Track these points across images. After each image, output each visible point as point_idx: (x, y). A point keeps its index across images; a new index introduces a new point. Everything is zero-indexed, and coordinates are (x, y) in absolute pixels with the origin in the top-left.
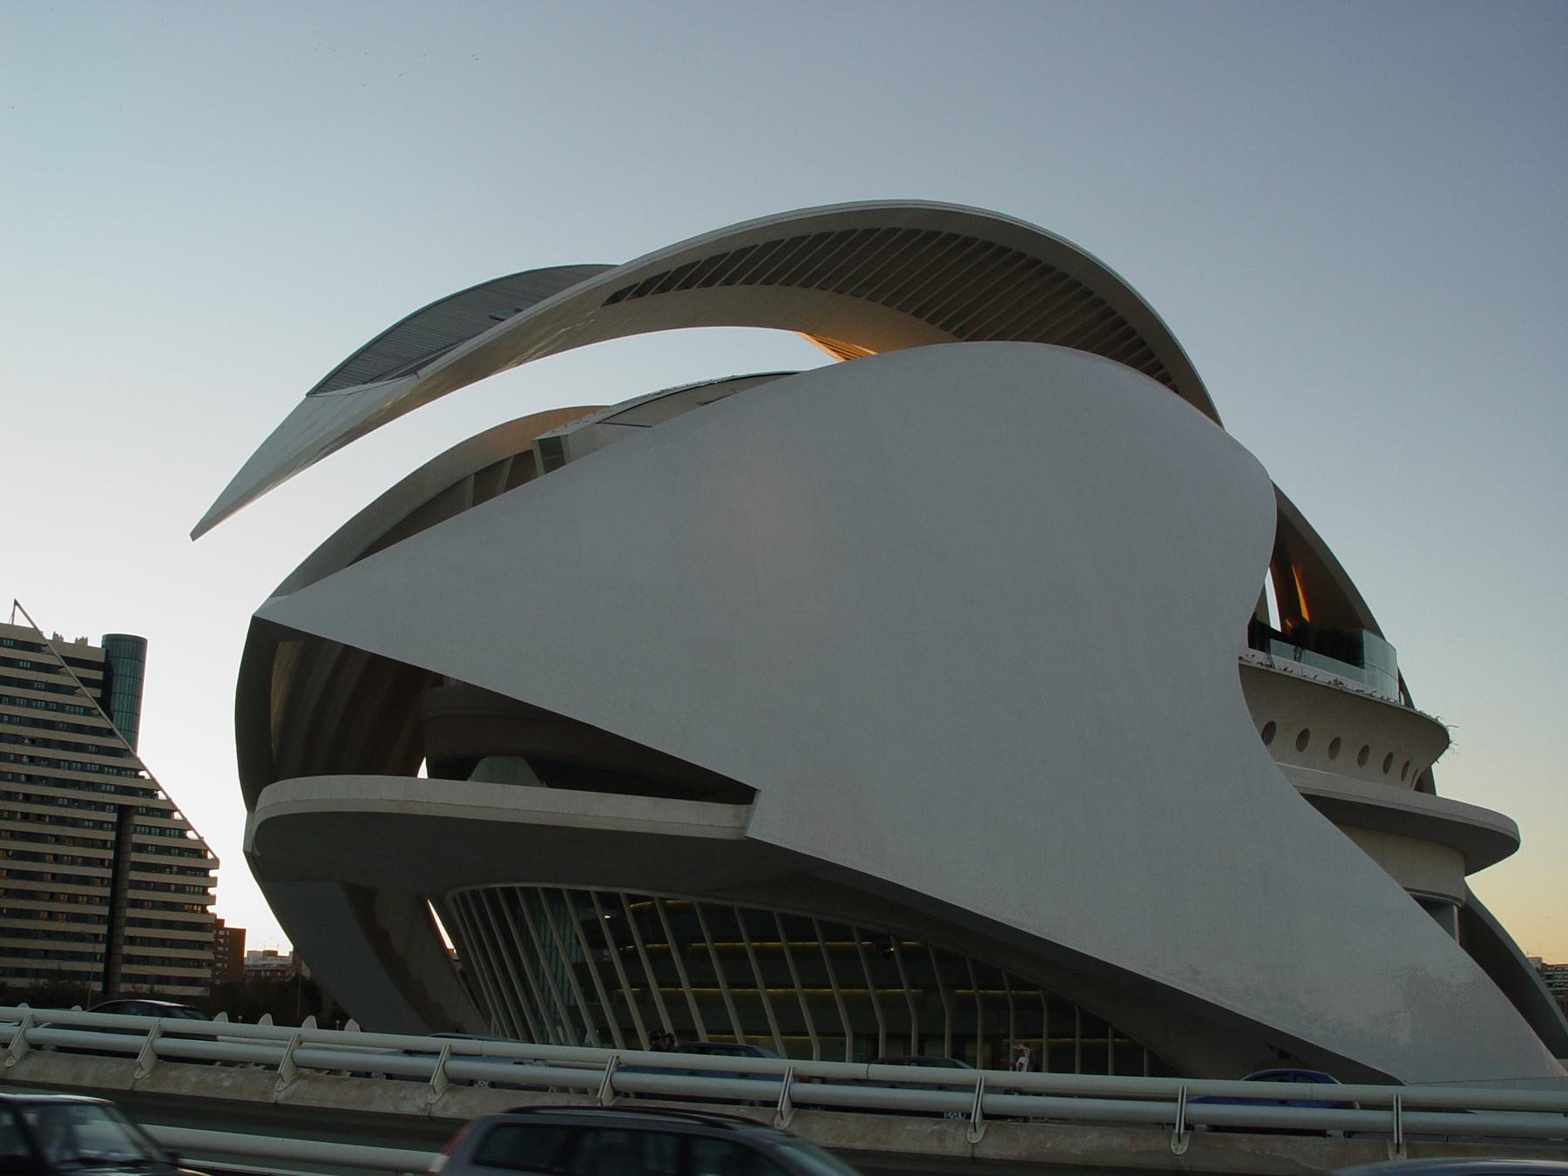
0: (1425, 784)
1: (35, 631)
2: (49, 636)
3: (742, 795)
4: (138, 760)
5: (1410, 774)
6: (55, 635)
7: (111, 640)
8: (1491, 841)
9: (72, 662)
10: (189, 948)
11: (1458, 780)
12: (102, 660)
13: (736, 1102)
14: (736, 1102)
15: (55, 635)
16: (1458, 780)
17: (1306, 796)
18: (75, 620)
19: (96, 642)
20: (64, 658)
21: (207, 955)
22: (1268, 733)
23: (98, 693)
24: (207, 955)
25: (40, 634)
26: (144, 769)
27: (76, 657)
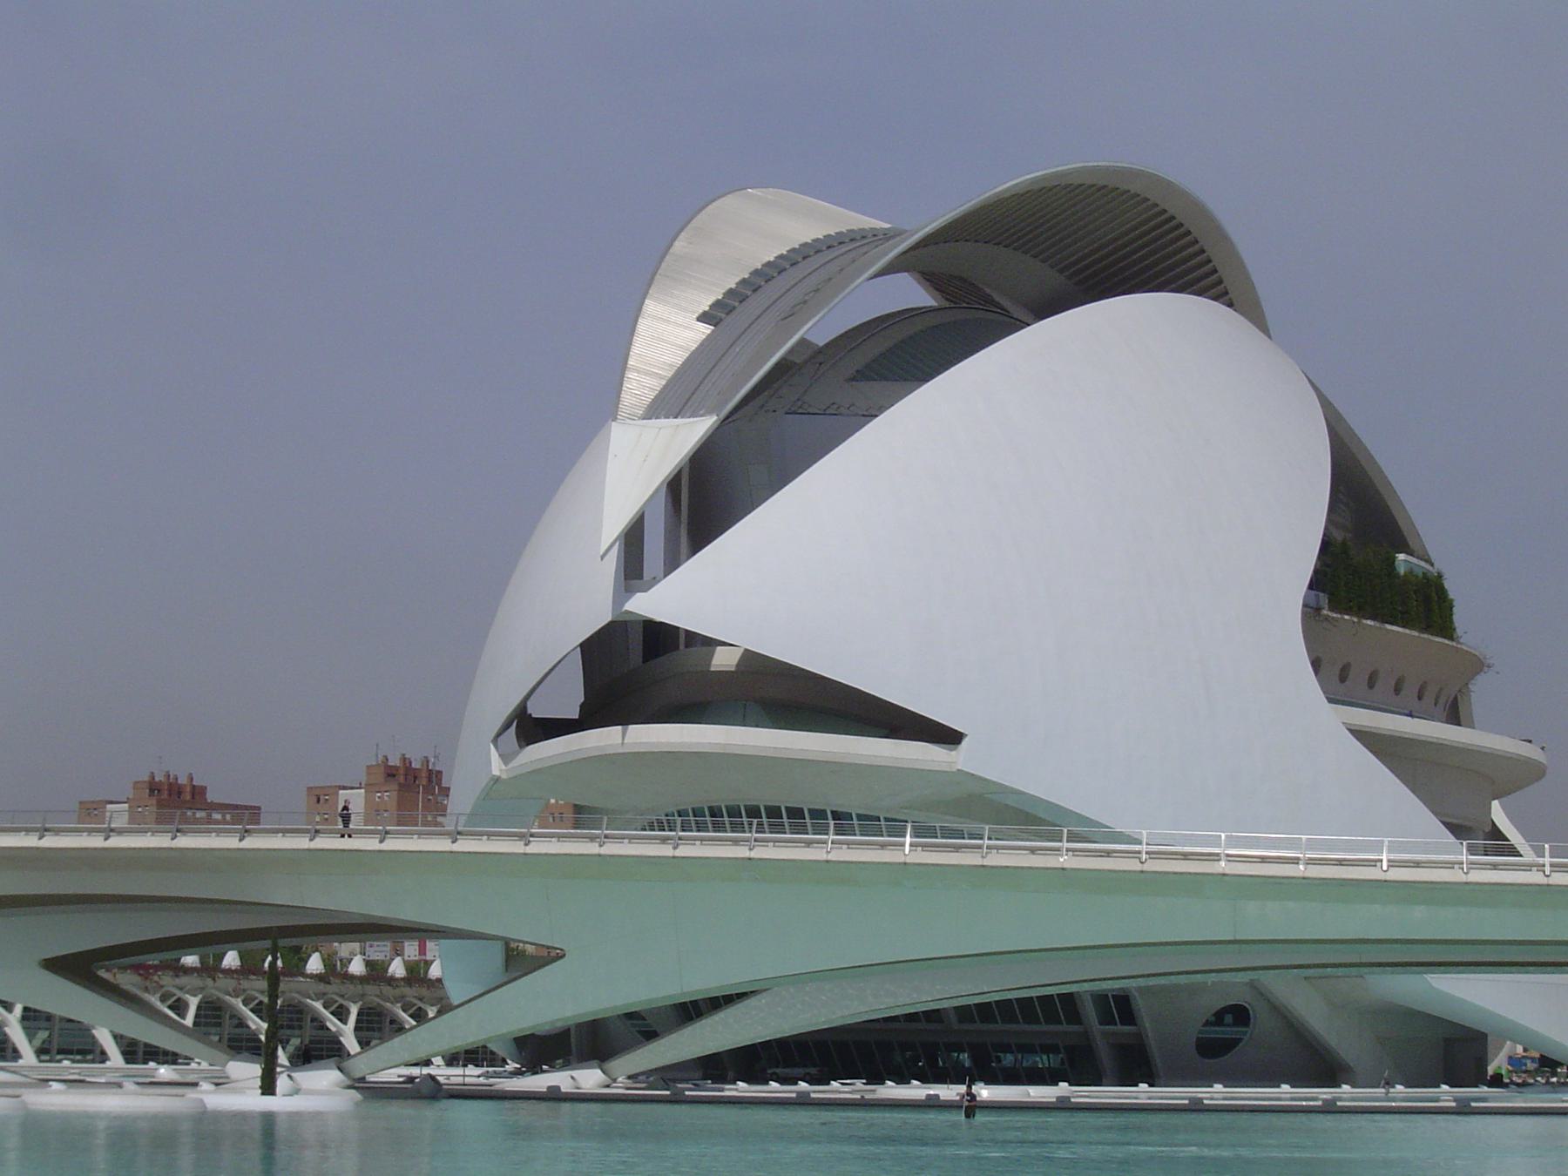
3: (948, 737)
5: (1442, 701)
6: (404, 759)
15: (404, 759)
17: (1351, 731)
22: (1316, 665)
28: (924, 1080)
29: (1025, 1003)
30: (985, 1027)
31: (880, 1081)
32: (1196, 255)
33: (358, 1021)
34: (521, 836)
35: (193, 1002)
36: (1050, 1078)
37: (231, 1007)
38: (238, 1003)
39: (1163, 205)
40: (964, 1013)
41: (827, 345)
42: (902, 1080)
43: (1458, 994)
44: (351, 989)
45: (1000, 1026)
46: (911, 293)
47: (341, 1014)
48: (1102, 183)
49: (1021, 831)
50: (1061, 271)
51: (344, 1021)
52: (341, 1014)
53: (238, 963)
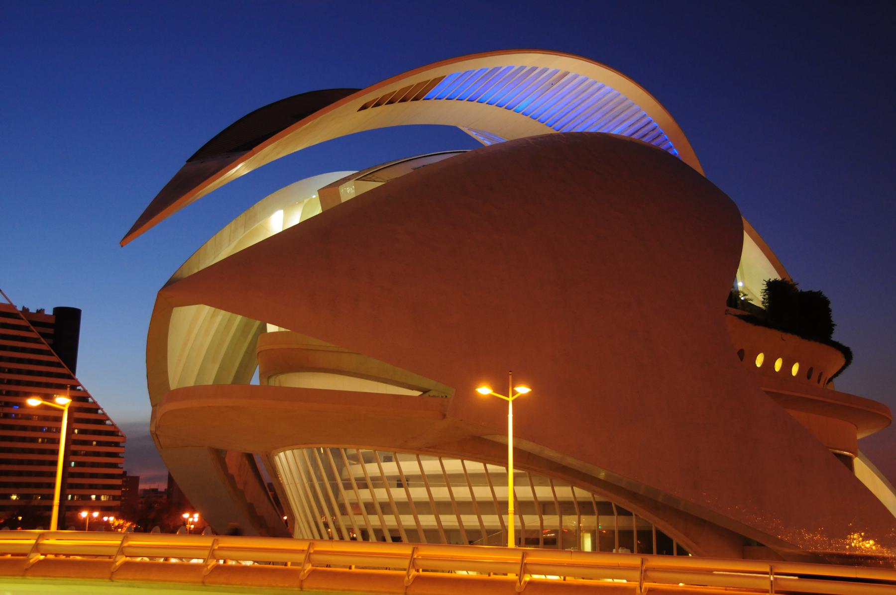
1: (11, 306)
2: (20, 308)
4: (76, 380)
6: (24, 308)
7: (58, 311)
9: (35, 324)
10: (96, 485)
12: (173, 385)
13: (637, 131)
14: (637, 131)
15: (24, 308)
18: (39, 298)
19: (49, 312)
20: (30, 321)
21: (118, 482)
23: (51, 341)
24: (118, 482)
25: (14, 307)
26: (80, 385)
27: (36, 320)
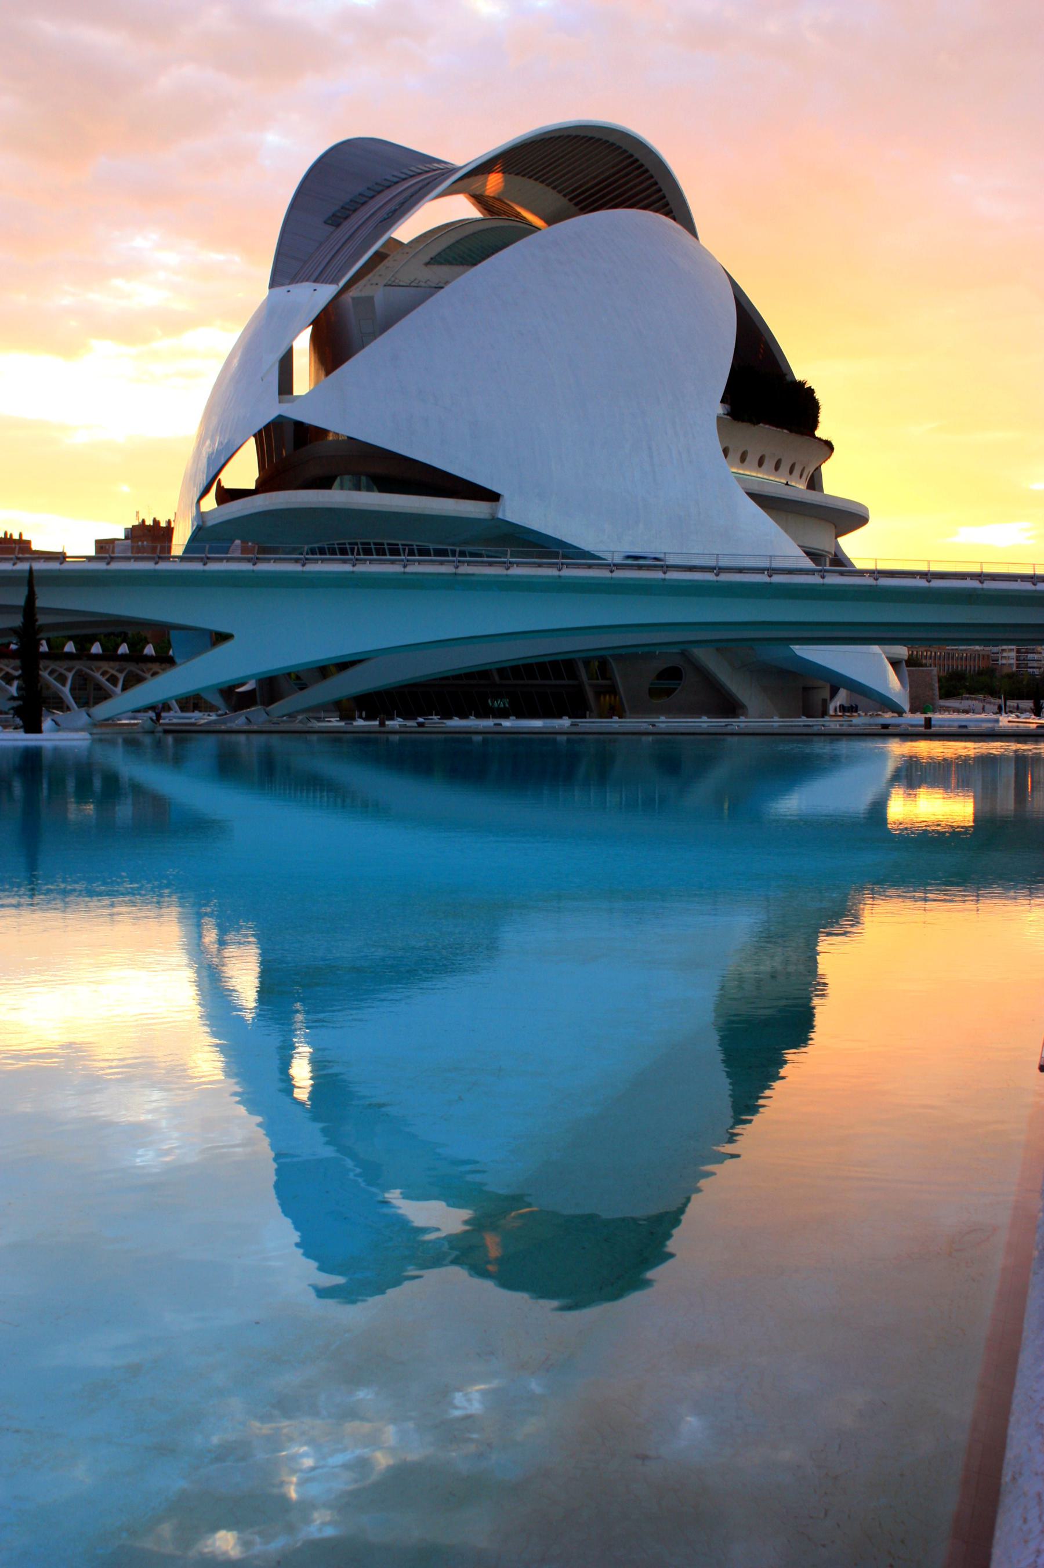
0: (815, 482)
3: (493, 497)
6: (155, 520)
8: (852, 518)
11: (838, 481)
15: (155, 520)
16: (838, 481)
17: (749, 494)
22: (726, 452)
28: (478, 716)
29: (541, 665)
30: (558, 682)
31: (449, 717)
32: (648, 179)
33: (72, 684)
34: (201, 559)
35: (70, 676)
36: (504, 714)
37: (93, 678)
38: (98, 675)
39: (631, 151)
40: (501, 671)
41: (412, 242)
42: (464, 716)
43: (810, 658)
44: (67, 664)
45: (539, 682)
46: (459, 208)
47: (62, 679)
48: (590, 135)
49: (522, 552)
50: (565, 196)
51: (64, 685)
52: (62, 679)
53: (100, 651)
